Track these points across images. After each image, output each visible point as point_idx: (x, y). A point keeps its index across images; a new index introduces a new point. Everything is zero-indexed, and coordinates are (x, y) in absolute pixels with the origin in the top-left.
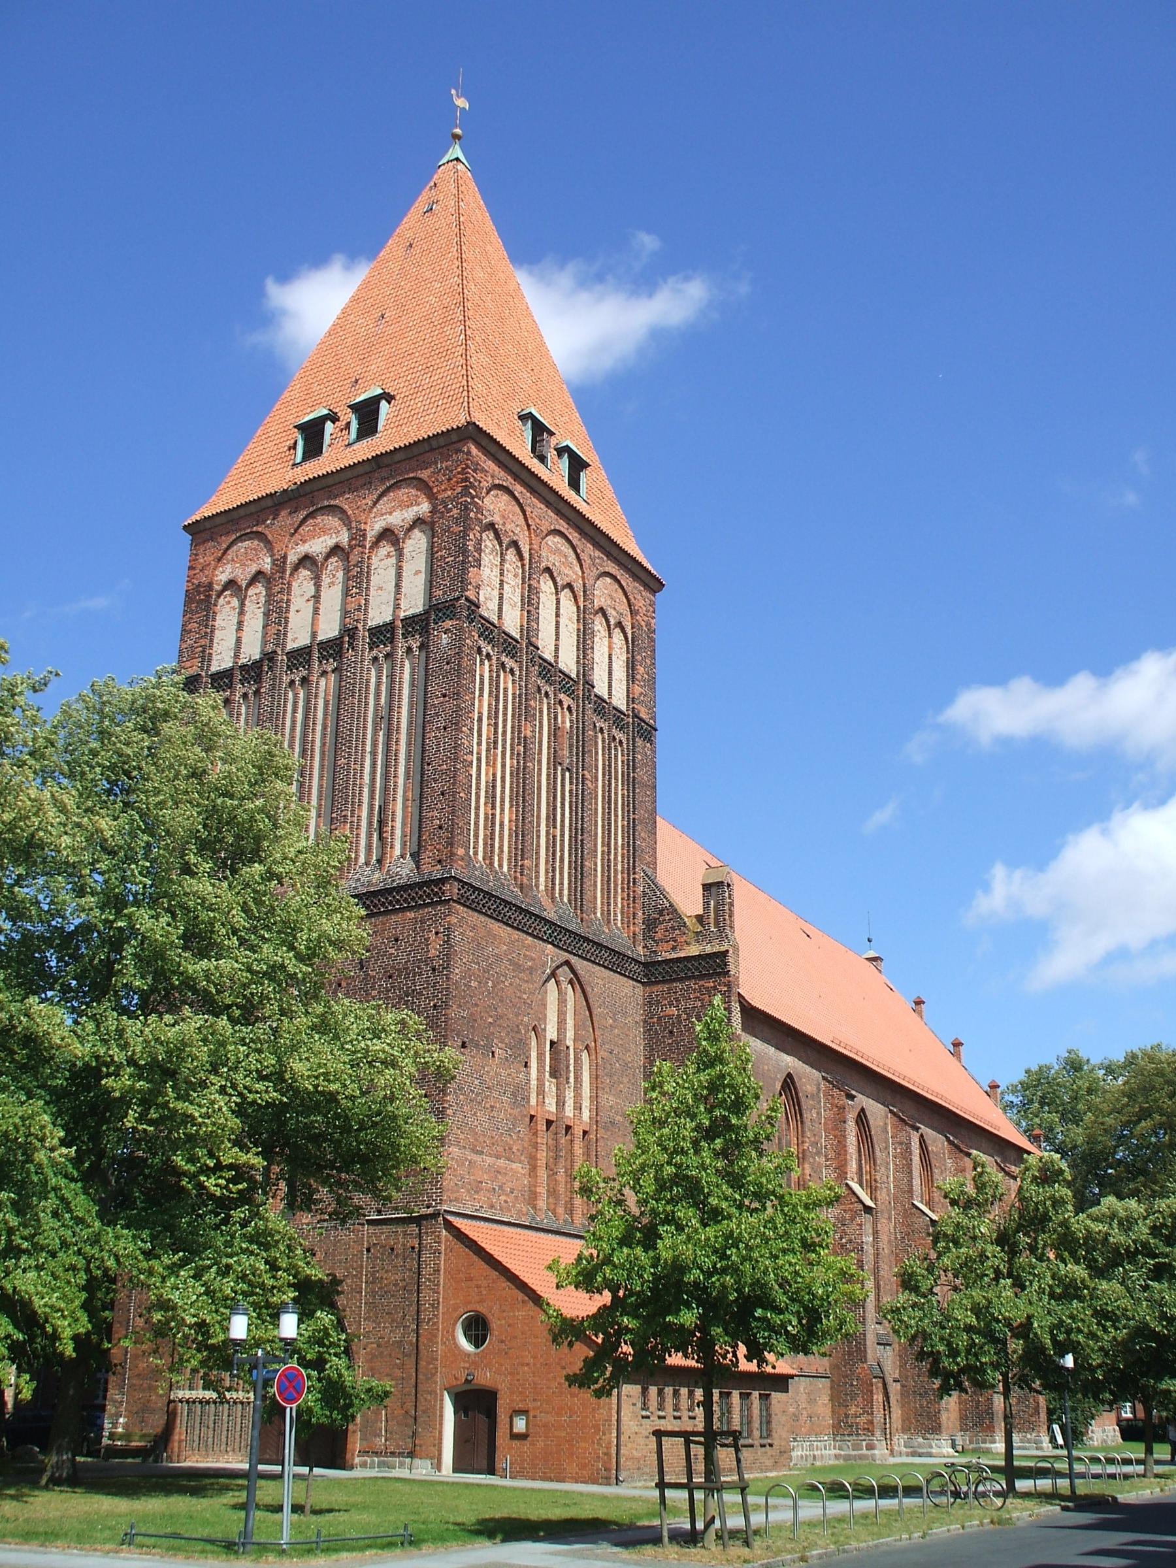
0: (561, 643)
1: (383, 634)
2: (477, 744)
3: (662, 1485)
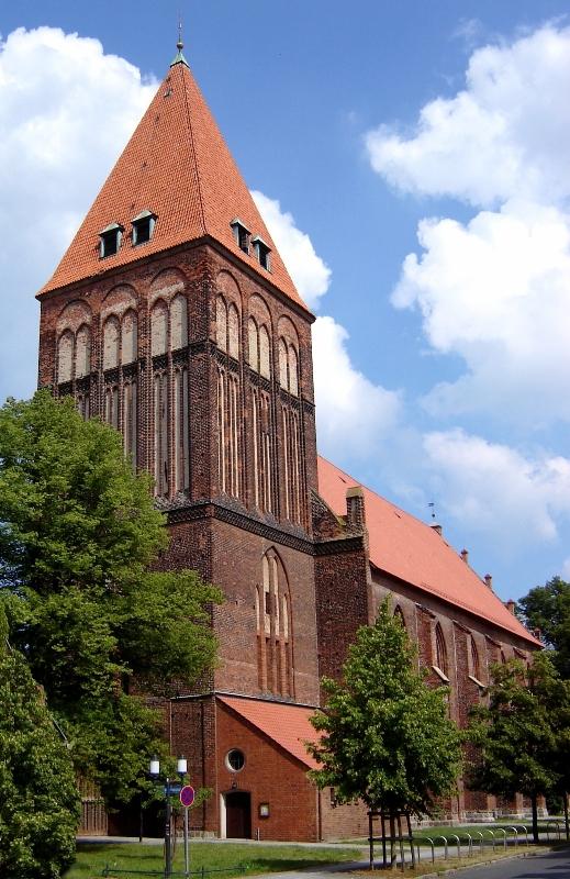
1: (161, 361)
2: (219, 425)
3: (371, 841)
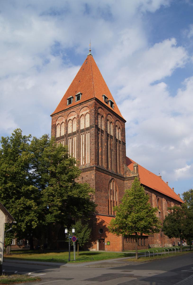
0: (60, 132)
